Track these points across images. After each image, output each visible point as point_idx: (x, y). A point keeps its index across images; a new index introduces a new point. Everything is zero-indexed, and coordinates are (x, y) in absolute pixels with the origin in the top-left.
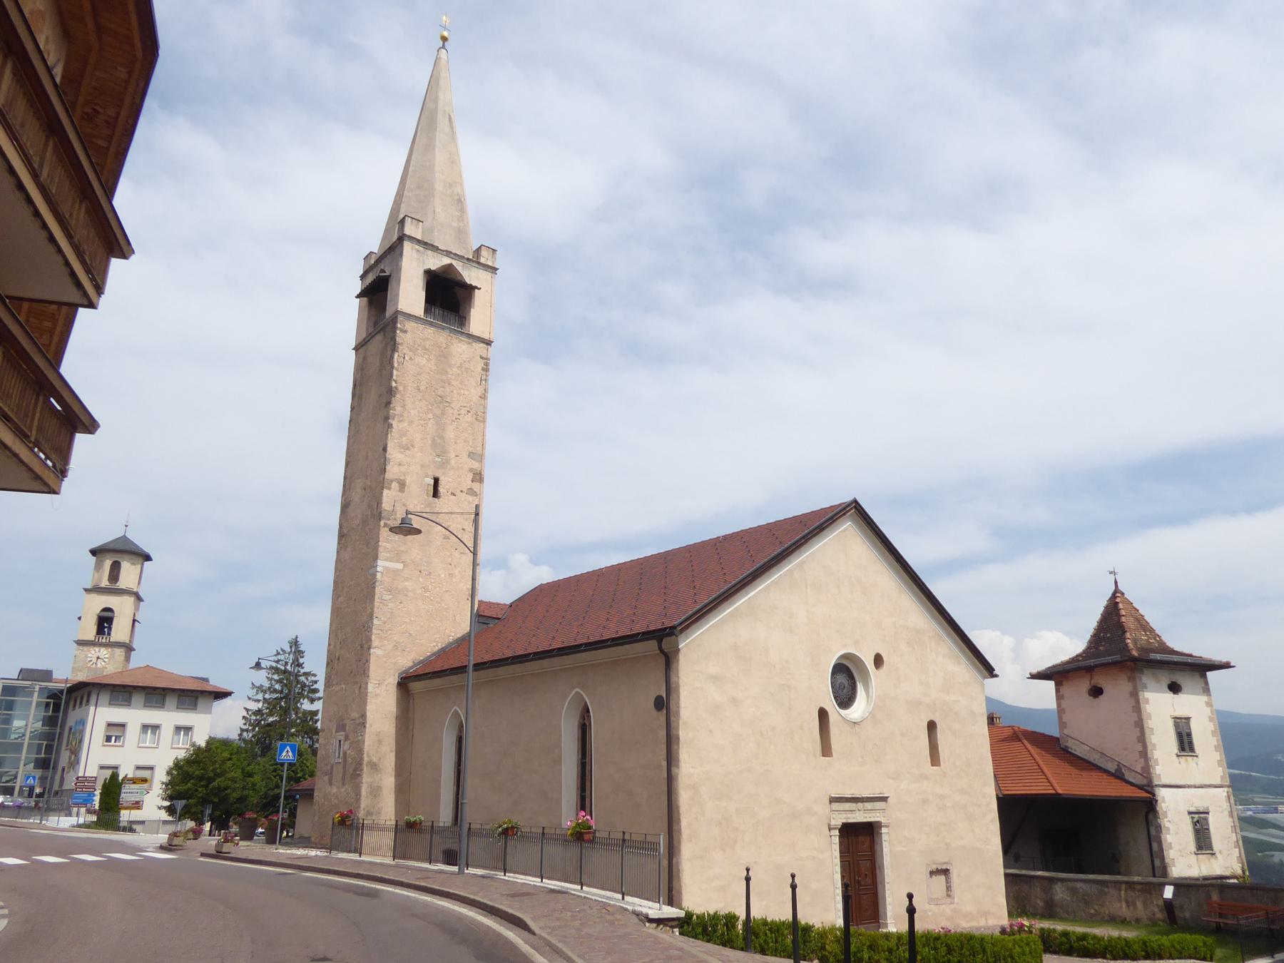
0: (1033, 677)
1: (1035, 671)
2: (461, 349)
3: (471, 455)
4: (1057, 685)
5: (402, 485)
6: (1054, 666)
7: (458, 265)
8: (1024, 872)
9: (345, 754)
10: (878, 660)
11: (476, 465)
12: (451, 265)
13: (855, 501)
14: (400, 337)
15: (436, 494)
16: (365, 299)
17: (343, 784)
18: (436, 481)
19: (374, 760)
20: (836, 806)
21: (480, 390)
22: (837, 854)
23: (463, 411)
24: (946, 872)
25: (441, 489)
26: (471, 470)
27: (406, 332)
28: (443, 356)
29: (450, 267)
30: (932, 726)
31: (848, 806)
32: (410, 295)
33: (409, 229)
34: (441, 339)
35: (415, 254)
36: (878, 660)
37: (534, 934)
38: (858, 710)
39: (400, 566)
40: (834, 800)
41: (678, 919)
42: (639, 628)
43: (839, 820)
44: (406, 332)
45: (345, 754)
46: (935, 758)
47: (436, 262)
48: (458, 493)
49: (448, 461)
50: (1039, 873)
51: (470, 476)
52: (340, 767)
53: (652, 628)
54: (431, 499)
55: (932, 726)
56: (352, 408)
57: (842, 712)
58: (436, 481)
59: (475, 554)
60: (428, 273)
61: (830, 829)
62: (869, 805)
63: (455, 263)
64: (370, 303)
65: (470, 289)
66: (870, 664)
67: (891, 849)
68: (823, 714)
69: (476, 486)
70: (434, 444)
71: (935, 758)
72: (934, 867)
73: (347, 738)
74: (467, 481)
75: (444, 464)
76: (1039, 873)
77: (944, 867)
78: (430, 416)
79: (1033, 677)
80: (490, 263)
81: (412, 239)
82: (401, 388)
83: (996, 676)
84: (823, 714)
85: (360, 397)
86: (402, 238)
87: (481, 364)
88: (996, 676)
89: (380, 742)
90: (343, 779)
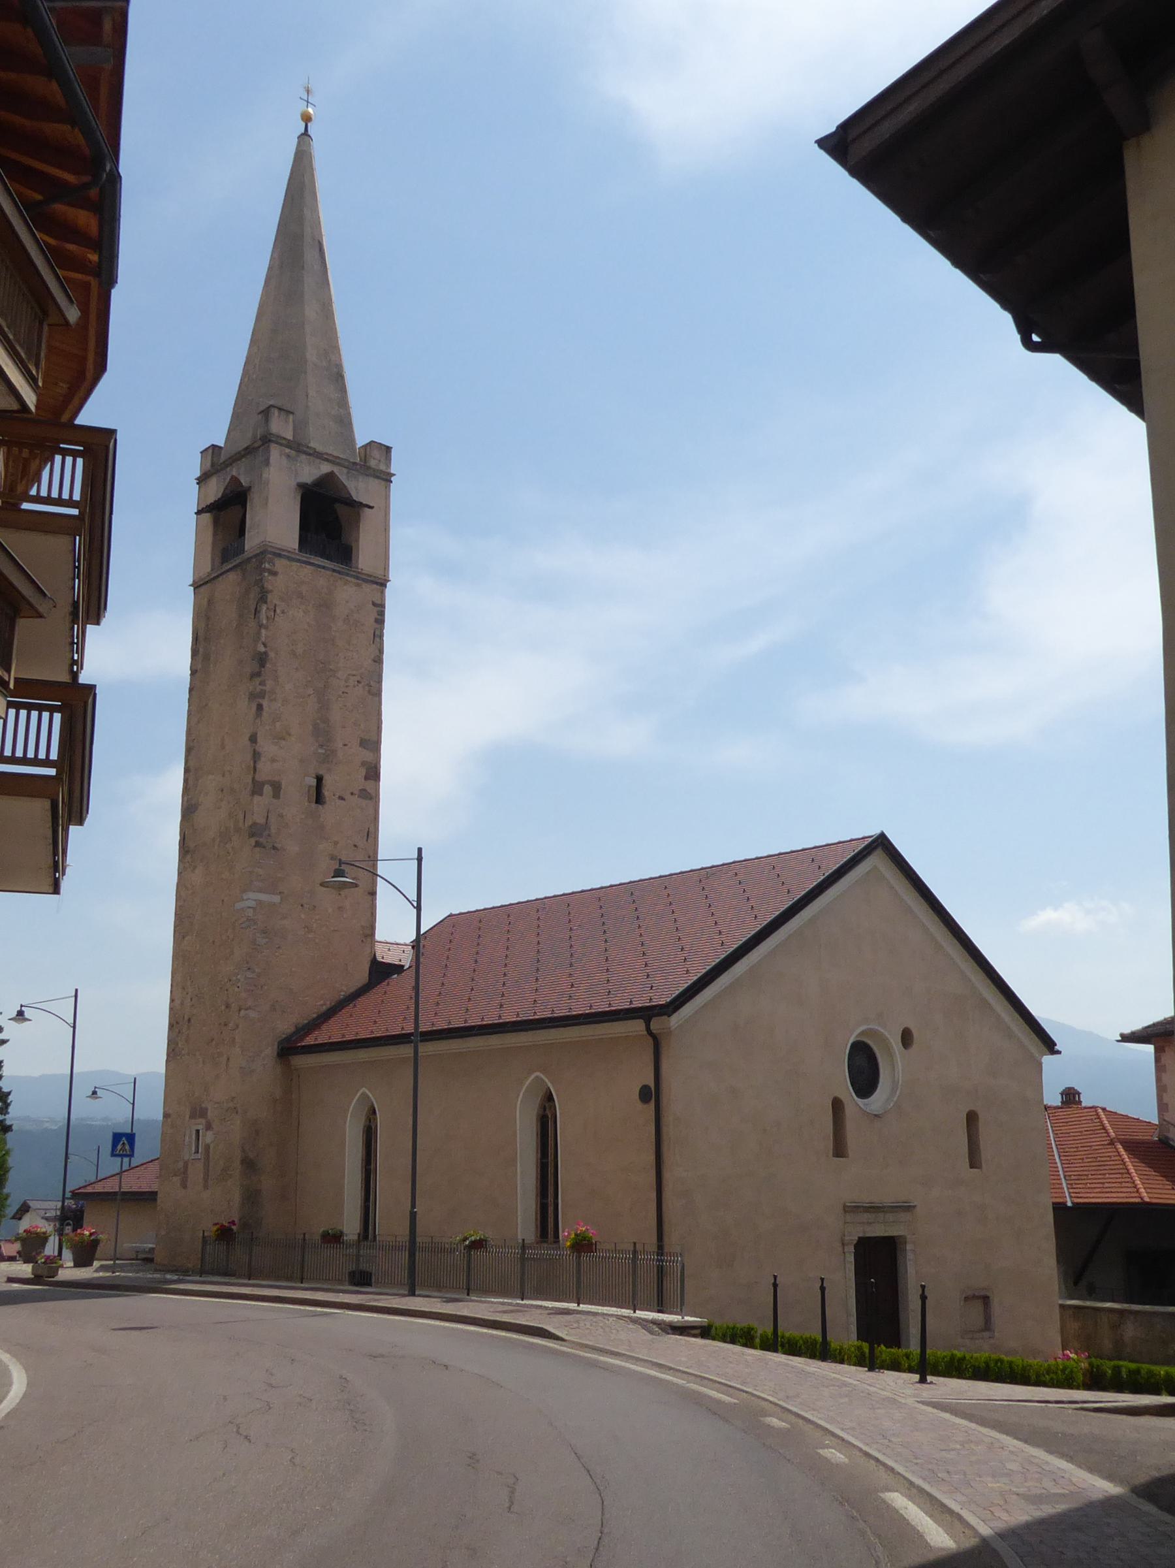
0: (1125, 1038)
1: (1127, 1031)
2: (347, 594)
4: (1159, 1051)
5: (277, 788)
6: (1154, 1025)
8: (1088, 1304)
9: (207, 1147)
10: (907, 1038)
11: (368, 756)
12: (332, 473)
13: (882, 836)
14: (270, 582)
15: (319, 799)
16: (207, 517)
17: (206, 1187)
18: (320, 779)
20: (849, 1217)
22: (852, 1275)
24: (986, 1300)
25: (326, 793)
26: (363, 764)
27: (275, 574)
28: (325, 605)
29: (331, 476)
30: (972, 1118)
31: (866, 1217)
32: (276, 521)
33: (280, 427)
35: (284, 461)
36: (907, 1038)
37: (563, 1340)
38: (878, 1100)
39: (276, 899)
40: (847, 1209)
41: (701, 1327)
42: (620, 1004)
43: (855, 1233)
44: (275, 574)
45: (207, 1147)
46: (974, 1161)
47: (310, 472)
48: (347, 796)
50: (1108, 1305)
51: (363, 772)
52: (200, 1166)
53: (636, 1004)
54: (314, 805)
55: (972, 1118)
56: (194, 672)
57: (860, 1101)
58: (320, 779)
60: (302, 486)
62: (890, 1217)
63: (336, 470)
64: (216, 522)
65: (356, 507)
67: (915, 1271)
68: (837, 1106)
69: (369, 785)
71: (974, 1161)
72: (970, 1293)
73: (209, 1127)
74: (359, 782)
75: (328, 757)
76: (1108, 1305)
77: (982, 1293)
78: (310, 691)
79: (1125, 1038)
80: (382, 467)
81: (280, 440)
82: (272, 655)
83: (1059, 1052)
84: (837, 1106)
85: (206, 658)
86: (267, 440)
87: (374, 615)
88: (1059, 1052)
89: (257, 1132)
90: (206, 1180)
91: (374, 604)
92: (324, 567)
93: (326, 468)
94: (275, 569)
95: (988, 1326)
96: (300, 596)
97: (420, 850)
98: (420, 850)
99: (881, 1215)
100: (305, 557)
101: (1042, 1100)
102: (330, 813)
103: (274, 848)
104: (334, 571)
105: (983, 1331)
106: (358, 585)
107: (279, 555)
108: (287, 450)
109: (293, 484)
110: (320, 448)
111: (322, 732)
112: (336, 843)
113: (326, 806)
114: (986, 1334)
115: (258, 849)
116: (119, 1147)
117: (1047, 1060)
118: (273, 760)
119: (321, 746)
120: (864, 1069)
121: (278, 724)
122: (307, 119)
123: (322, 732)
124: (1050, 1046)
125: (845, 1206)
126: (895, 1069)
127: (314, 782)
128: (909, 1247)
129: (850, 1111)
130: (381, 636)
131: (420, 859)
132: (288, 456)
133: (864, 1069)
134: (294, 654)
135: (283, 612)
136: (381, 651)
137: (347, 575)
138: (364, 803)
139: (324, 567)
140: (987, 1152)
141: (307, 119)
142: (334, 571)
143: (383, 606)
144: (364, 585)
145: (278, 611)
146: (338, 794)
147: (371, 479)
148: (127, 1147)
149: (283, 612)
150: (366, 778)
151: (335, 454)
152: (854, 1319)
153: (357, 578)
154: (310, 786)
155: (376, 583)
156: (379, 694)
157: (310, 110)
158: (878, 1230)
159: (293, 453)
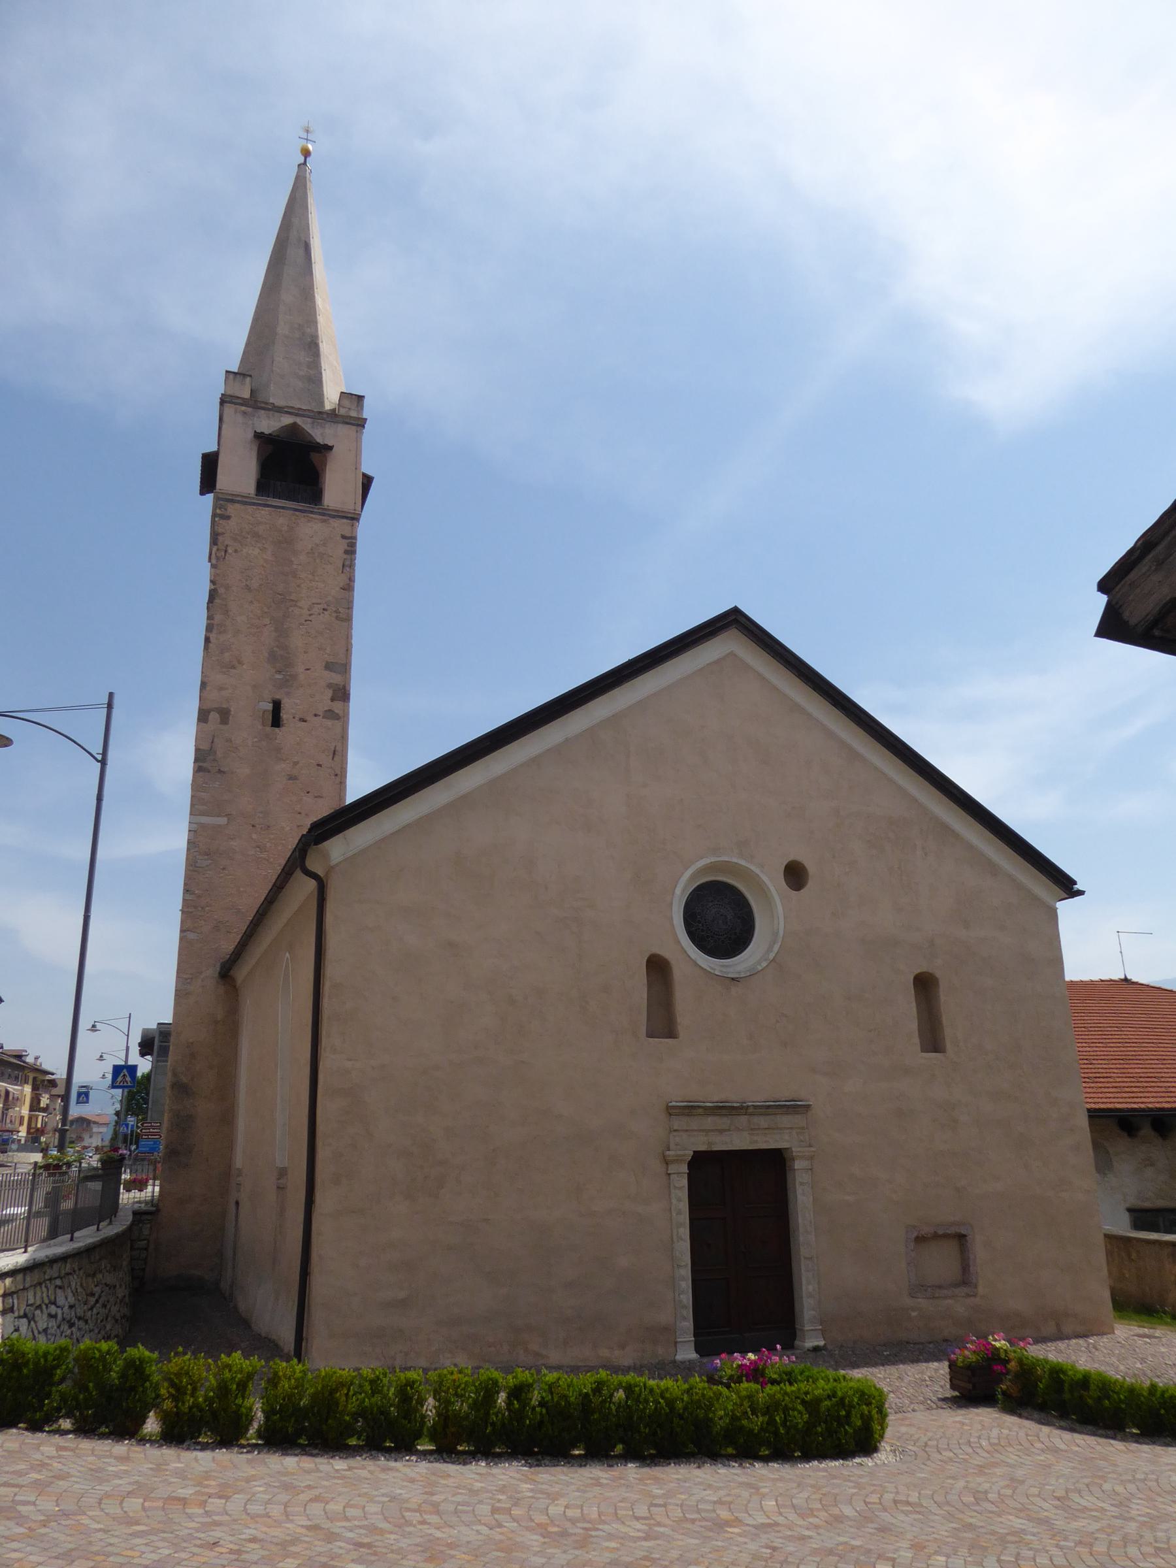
2: (311, 530)
3: (329, 666)
7: (306, 424)
11: (336, 678)
12: (295, 424)
15: (276, 721)
19: (185, 1080)
20: (677, 1123)
21: (342, 579)
23: (316, 609)
24: (961, 1238)
25: (284, 715)
26: (330, 686)
27: (228, 518)
28: (286, 542)
30: (925, 985)
31: (709, 1122)
34: (281, 521)
35: (240, 419)
39: (222, 821)
44: (228, 518)
46: (932, 1039)
47: (270, 424)
49: (294, 677)
51: (329, 693)
54: (269, 729)
59: (103, 763)
61: (667, 1162)
63: (299, 421)
66: (774, 883)
68: (658, 968)
69: (337, 706)
70: (273, 657)
74: (324, 700)
75: (288, 681)
77: (952, 1230)
78: (267, 621)
80: (353, 414)
83: (1080, 893)
84: (658, 968)
87: (343, 545)
88: (1080, 893)
91: (344, 537)
92: (283, 508)
93: (287, 420)
94: (228, 513)
95: (965, 1278)
96: (256, 535)
97: (111, 695)
98: (111, 695)
99: (744, 1119)
100: (262, 499)
101: (1056, 961)
102: (289, 734)
103: (220, 771)
104: (296, 510)
105: (956, 1285)
106: (324, 521)
107: (232, 501)
108: (243, 408)
109: (250, 435)
110: (280, 403)
111: (281, 661)
112: (296, 763)
113: (283, 729)
114: (964, 1290)
115: (201, 774)
116: (119, 1079)
117: (1065, 908)
118: (221, 689)
119: (279, 672)
120: (719, 917)
121: (227, 654)
122: (306, 153)
123: (281, 661)
124: (1067, 886)
125: (668, 1108)
126: (775, 915)
127: (270, 707)
128: (798, 1165)
129: (680, 973)
130: (352, 566)
131: (110, 706)
132: (245, 413)
133: (719, 917)
134: (248, 588)
135: (236, 551)
136: (351, 579)
137: (312, 512)
138: (329, 723)
139: (283, 508)
140: (953, 1025)
141: (306, 153)
142: (296, 510)
143: (355, 538)
144: (332, 520)
145: (230, 551)
146: (297, 717)
147: (340, 426)
148: (128, 1079)
149: (236, 551)
150: (332, 700)
151: (298, 406)
152: (686, 1272)
153: (324, 515)
154: (265, 711)
155: (347, 518)
156: (348, 619)
157: (310, 147)
158: (739, 1140)
159: (250, 410)
